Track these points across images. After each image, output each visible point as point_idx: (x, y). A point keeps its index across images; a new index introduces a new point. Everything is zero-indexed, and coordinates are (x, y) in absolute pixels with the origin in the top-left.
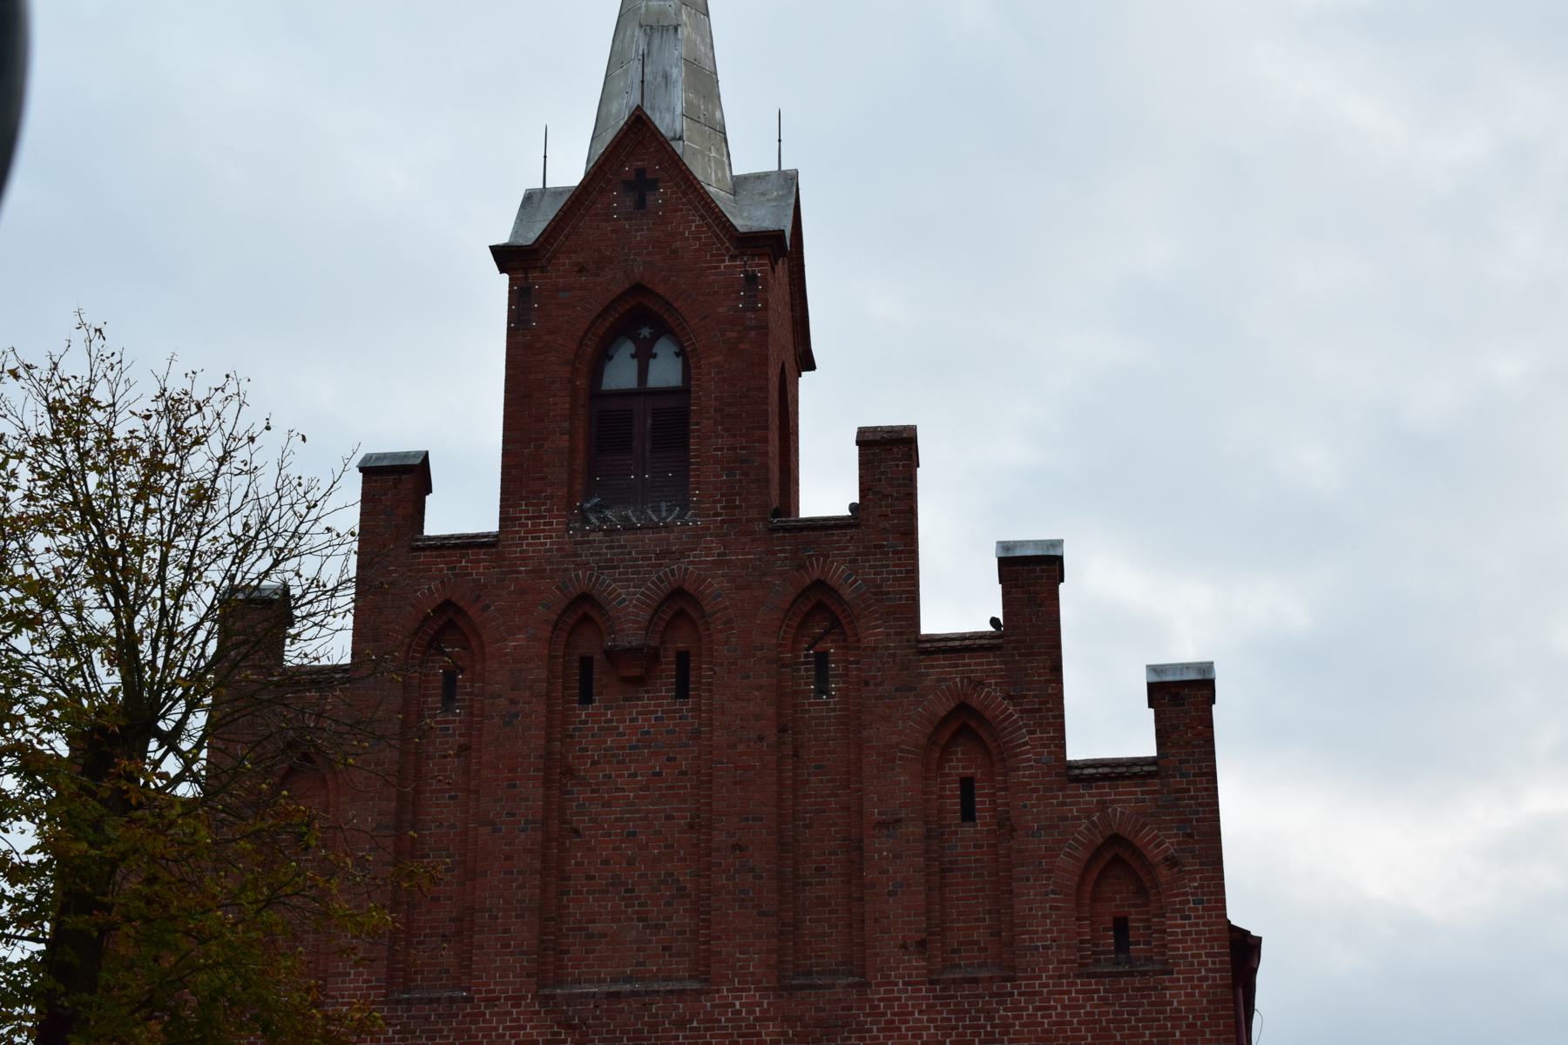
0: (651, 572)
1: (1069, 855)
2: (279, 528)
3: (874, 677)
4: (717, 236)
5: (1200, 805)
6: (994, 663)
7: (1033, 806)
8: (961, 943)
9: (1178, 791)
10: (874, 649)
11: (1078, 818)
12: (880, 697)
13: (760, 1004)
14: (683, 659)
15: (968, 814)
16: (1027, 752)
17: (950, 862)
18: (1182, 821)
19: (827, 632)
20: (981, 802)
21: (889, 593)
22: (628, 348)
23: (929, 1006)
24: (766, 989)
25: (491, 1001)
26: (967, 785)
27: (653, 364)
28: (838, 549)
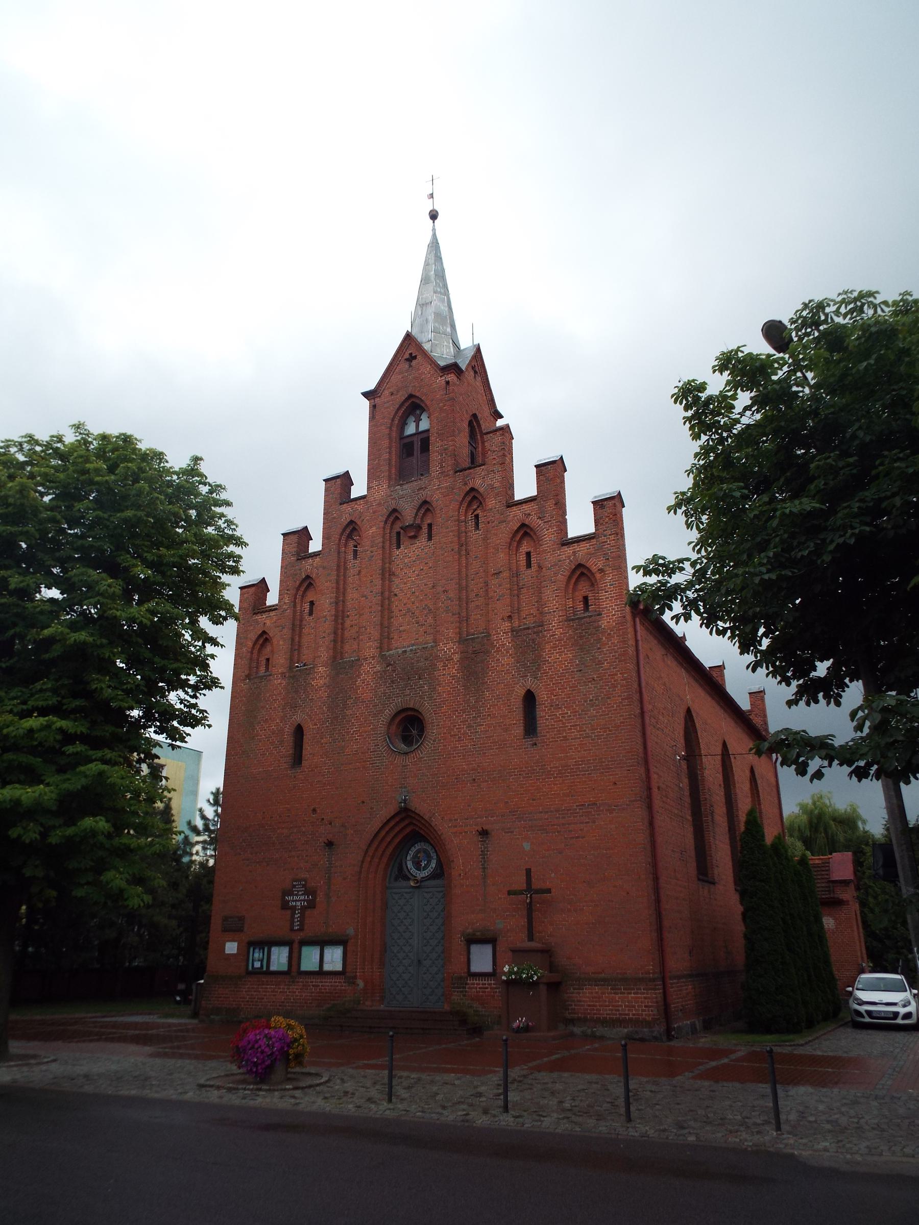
1: (561, 575)
3: (491, 520)
6: (534, 506)
7: (549, 558)
8: (526, 615)
10: (491, 509)
11: (565, 560)
12: (493, 527)
14: (430, 526)
15: (529, 565)
16: (546, 538)
17: (523, 585)
18: (604, 554)
19: (478, 507)
22: (412, 418)
25: (366, 659)
26: (528, 554)
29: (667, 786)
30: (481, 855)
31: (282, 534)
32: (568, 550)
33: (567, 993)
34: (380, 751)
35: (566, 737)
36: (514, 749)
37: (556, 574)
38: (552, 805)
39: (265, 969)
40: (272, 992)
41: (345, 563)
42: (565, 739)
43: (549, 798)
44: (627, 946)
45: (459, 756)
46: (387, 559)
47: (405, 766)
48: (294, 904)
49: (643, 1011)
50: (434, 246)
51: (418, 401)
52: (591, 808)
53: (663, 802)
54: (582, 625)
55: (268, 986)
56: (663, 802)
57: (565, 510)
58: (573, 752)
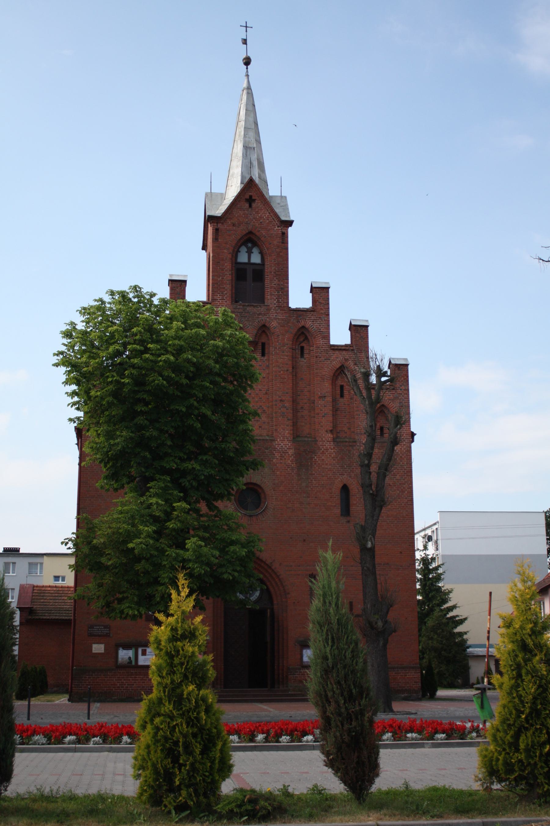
0: (256, 319)
3: (319, 355)
4: (274, 219)
9: (400, 394)
13: (288, 444)
19: (304, 341)
20: (346, 393)
21: (323, 332)
23: (333, 448)
24: (290, 440)
27: (252, 255)
28: (309, 317)
39: (133, 663)
40: (140, 680)
55: (137, 676)
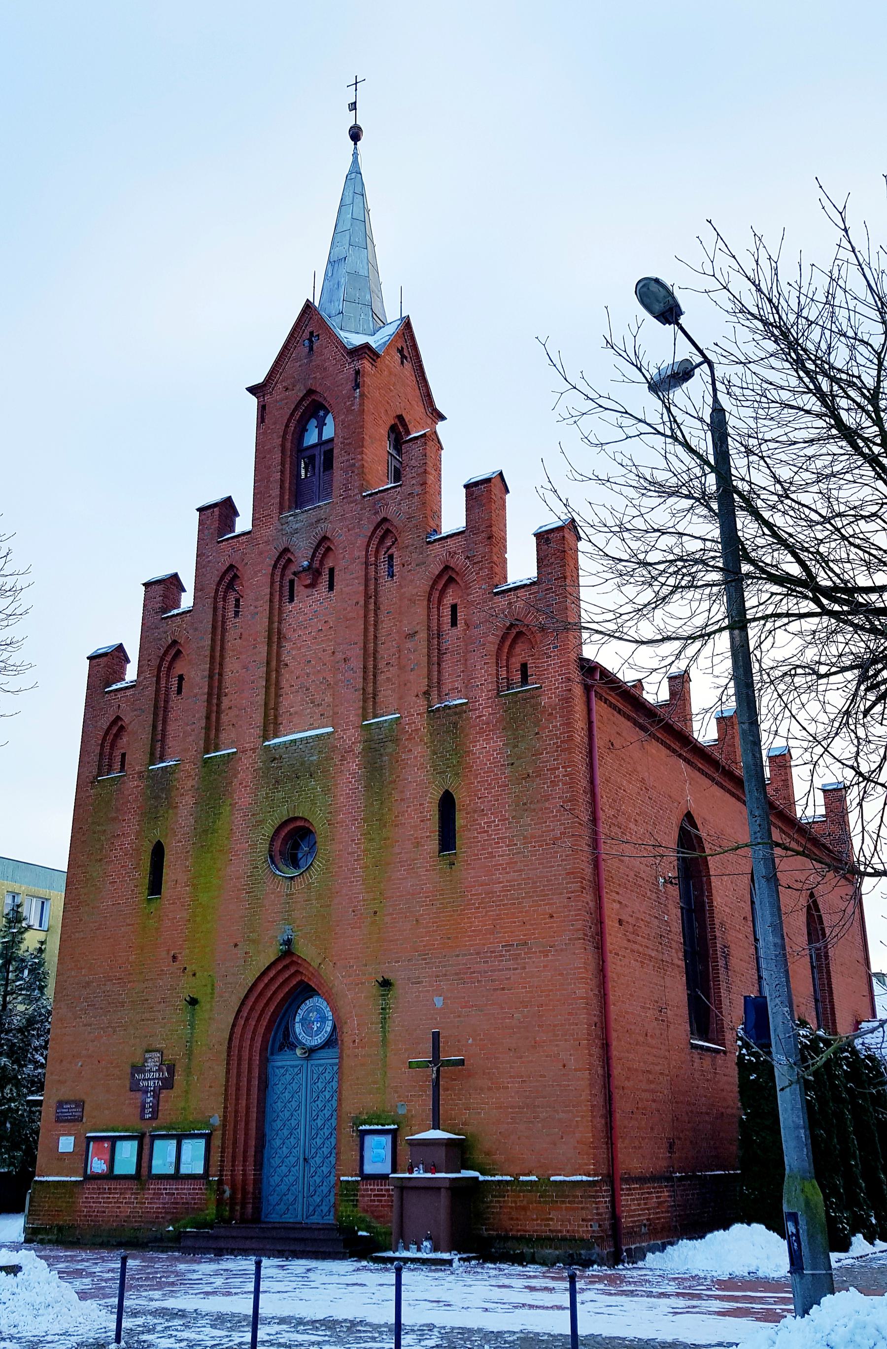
1: (493, 634)
2: (668, 578)
5: (557, 595)
15: (454, 623)
20: (460, 616)
22: (314, 422)
26: (454, 608)
29: (638, 918)
30: (381, 1014)
31: (144, 584)
32: (502, 601)
33: (484, 1202)
34: (259, 875)
35: (492, 853)
36: (426, 871)
37: (485, 635)
38: (471, 945)
41: (223, 623)
42: (492, 855)
43: (469, 936)
44: (562, 1138)
45: (357, 881)
46: (276, 617)
47: (291, 895)
48: (145, 1083)
49: (579, 1226)
50: (355, 172)
51: (321, 400)
52: (520, 949)
53: (629, 941)
54: (516, 702)
56: (629, 941)
57: (505, 547)
58: (500, 874)
